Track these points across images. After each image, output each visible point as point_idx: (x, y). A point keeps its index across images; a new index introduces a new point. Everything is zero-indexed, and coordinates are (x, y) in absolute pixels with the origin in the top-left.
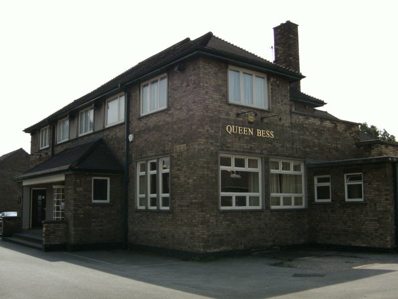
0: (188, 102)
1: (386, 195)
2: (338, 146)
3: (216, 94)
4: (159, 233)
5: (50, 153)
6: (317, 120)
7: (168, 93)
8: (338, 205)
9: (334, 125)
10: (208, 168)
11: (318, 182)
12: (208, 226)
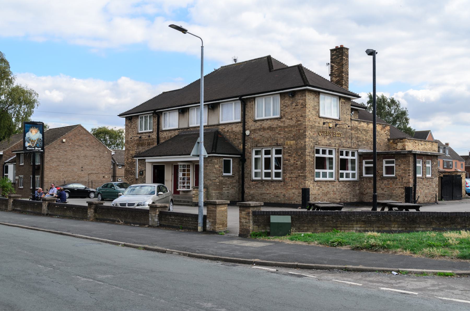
0: (297, 115)
7: (281, 108)
10: (309, 155)
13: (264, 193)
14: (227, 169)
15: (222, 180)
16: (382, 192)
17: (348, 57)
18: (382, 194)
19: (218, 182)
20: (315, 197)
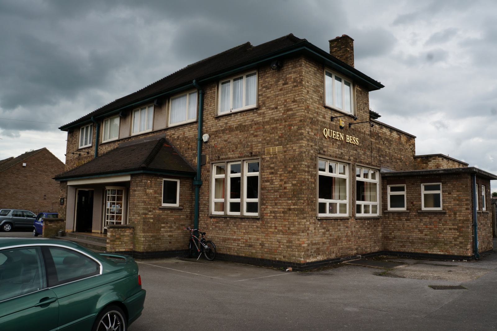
0: (286, 101)
1: (467, 205)
2: (402, 157)
3: (315, 95)
4: (242, 240)
5: (93, 152)
6: (388, 130)
7: (258, 91)
8: (414, 214)
9: (399, 136)
10: (308, 172)
11: (425, 190)
12: (308, 234)
13: (229, 239)
14: (170, 196)
15: (159, 215)
16: (420, 236)
17: (353, 50)
18: (420, 239)
19: (152, 218)
20: (318, 249)
